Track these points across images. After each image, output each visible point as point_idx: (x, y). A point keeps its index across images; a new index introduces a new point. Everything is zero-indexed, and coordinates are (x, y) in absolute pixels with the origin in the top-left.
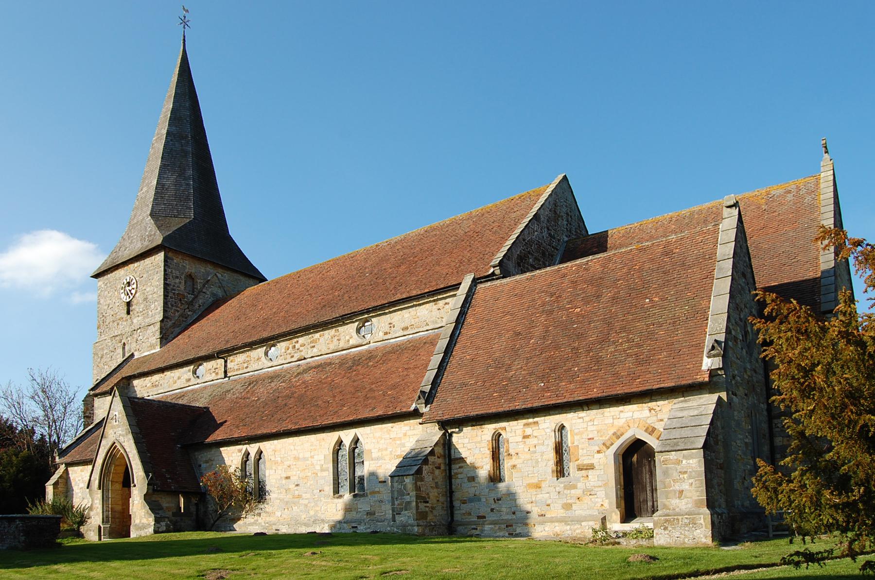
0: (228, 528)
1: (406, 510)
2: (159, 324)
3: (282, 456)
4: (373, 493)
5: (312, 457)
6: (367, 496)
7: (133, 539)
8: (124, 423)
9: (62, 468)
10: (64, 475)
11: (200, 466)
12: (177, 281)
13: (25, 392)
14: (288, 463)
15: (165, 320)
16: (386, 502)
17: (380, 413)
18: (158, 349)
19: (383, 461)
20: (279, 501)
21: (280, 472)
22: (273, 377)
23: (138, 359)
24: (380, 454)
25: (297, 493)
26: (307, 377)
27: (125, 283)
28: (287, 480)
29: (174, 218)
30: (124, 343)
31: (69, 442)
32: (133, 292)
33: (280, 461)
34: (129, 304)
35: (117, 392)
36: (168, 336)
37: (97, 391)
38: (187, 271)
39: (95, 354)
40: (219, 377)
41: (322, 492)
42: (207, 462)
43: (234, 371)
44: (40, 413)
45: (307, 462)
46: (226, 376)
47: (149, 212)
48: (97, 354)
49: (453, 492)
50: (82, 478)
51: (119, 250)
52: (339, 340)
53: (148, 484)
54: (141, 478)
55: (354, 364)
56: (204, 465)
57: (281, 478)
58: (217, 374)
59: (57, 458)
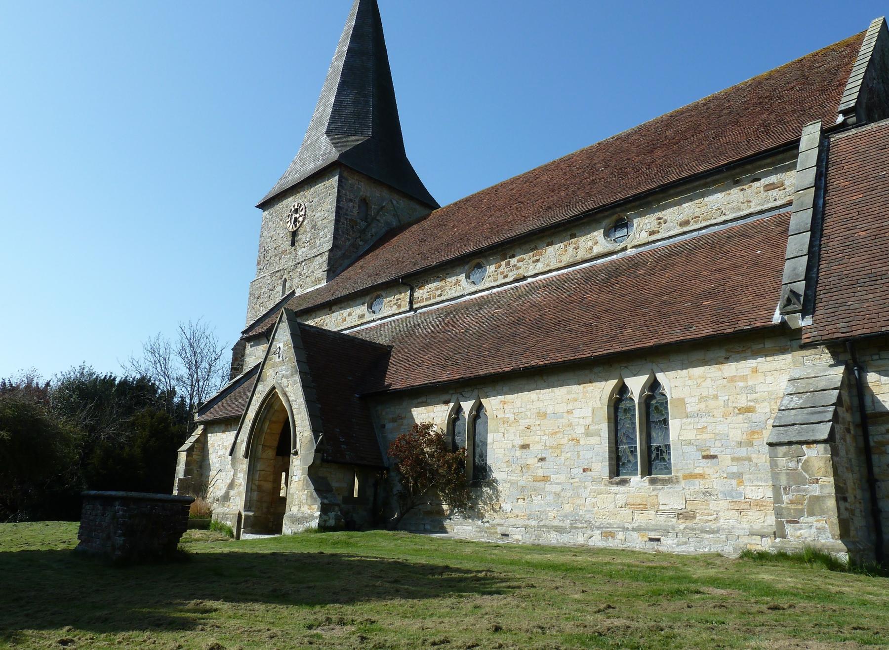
0: (422, 527)
1: (811, 514)
2: (327, 254)
3: (516, 411)
4: (690, 476)
5: (569, 412)
6: (678, 482)
7: (295, 537)
8: (290, 359)
9: (199, 431)
10: (202, 439)
11: (384, 426)
12: (351, 204)
13: (173, 346)
14: (526, 422)
15: (335, 249)
16: (720, 496)
17: (707, 331)
18: (324, 284)
19: (712, 419)
20: (508, 485)
21: (512, 437)
22: (480, 304)
23: (299, 296)
24: (702, 406)
25: (540, 473)
26: (537, 298)
27: (293, 210)
28: (524, 451)
29: (350, 137)
30: (285, 279)
31: (214, 394)
32: (301, 219)
33: (512, 419)
34: (294, 234)
35: (285, 314)
36: (336, 268)
37: (251, 334)
38: (361, 193)
39: (251, 294)
40: (402, 310)
41: (589, 473)
42: (394, 420)
43: (422, 301)
44: (184, 371)
45: (561, 420)
46: (411, 309)
47: (324, 130)
48: (254, 295)
49: (877, 480)
50: (223, 443)
51: (289, 175)
52: (576, 248)
53: (316, 451)
54: (306, 441)
55: (610, 277)
56: (389, 426)
57: (514, 446)
58: (399, 306)
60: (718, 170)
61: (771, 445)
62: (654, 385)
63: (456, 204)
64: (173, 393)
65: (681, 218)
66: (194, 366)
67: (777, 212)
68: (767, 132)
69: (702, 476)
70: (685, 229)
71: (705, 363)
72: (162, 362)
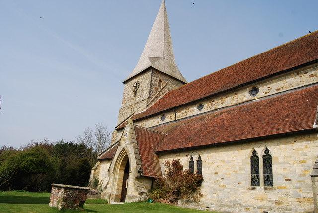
20: (209, 188)
24: (285, 160)
25: (222, 184)
26: (222, 117)
45: (230, 164)
59: (315, 124)
60: (291, 70)
61: (312, 176)
62: (267, 151)
63: (193, 82)
64: (92, 148)
65: (278, 87)
66: (100, 138)
67: (315, 85)
68: (310, 55)
69: (285, 188)
70: (279, 91)
71: (286, 143)
72: (89, 137)
